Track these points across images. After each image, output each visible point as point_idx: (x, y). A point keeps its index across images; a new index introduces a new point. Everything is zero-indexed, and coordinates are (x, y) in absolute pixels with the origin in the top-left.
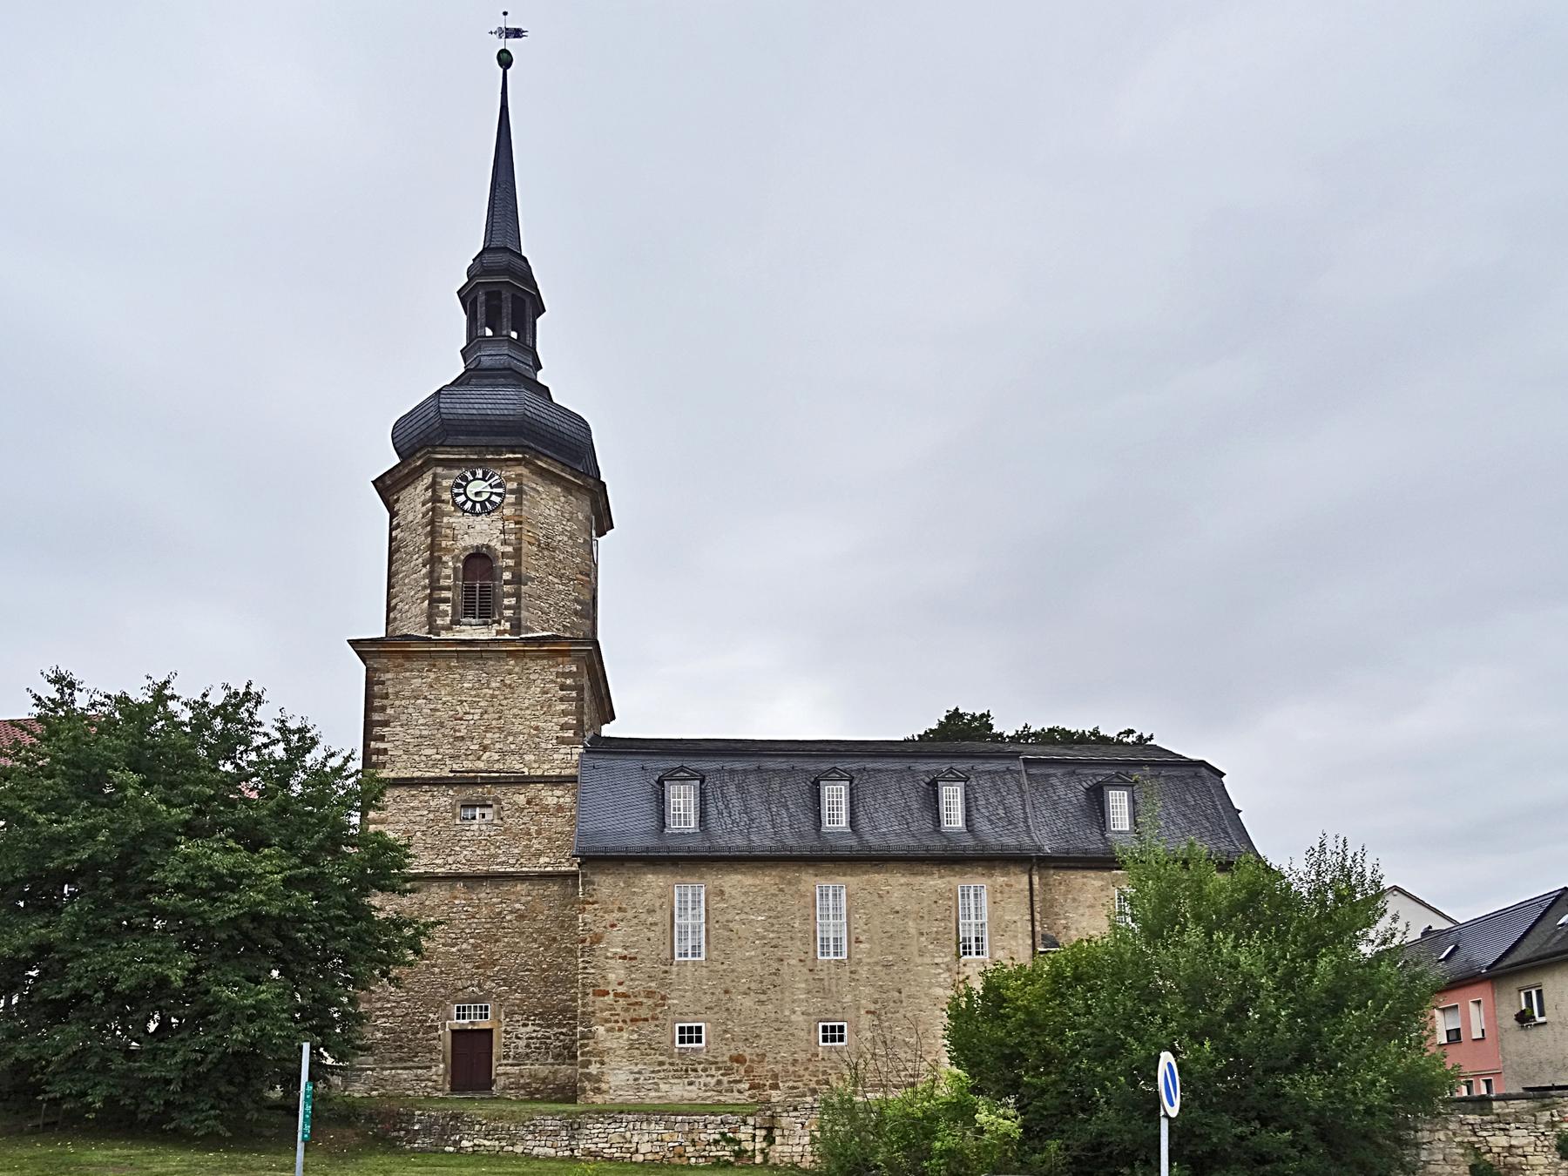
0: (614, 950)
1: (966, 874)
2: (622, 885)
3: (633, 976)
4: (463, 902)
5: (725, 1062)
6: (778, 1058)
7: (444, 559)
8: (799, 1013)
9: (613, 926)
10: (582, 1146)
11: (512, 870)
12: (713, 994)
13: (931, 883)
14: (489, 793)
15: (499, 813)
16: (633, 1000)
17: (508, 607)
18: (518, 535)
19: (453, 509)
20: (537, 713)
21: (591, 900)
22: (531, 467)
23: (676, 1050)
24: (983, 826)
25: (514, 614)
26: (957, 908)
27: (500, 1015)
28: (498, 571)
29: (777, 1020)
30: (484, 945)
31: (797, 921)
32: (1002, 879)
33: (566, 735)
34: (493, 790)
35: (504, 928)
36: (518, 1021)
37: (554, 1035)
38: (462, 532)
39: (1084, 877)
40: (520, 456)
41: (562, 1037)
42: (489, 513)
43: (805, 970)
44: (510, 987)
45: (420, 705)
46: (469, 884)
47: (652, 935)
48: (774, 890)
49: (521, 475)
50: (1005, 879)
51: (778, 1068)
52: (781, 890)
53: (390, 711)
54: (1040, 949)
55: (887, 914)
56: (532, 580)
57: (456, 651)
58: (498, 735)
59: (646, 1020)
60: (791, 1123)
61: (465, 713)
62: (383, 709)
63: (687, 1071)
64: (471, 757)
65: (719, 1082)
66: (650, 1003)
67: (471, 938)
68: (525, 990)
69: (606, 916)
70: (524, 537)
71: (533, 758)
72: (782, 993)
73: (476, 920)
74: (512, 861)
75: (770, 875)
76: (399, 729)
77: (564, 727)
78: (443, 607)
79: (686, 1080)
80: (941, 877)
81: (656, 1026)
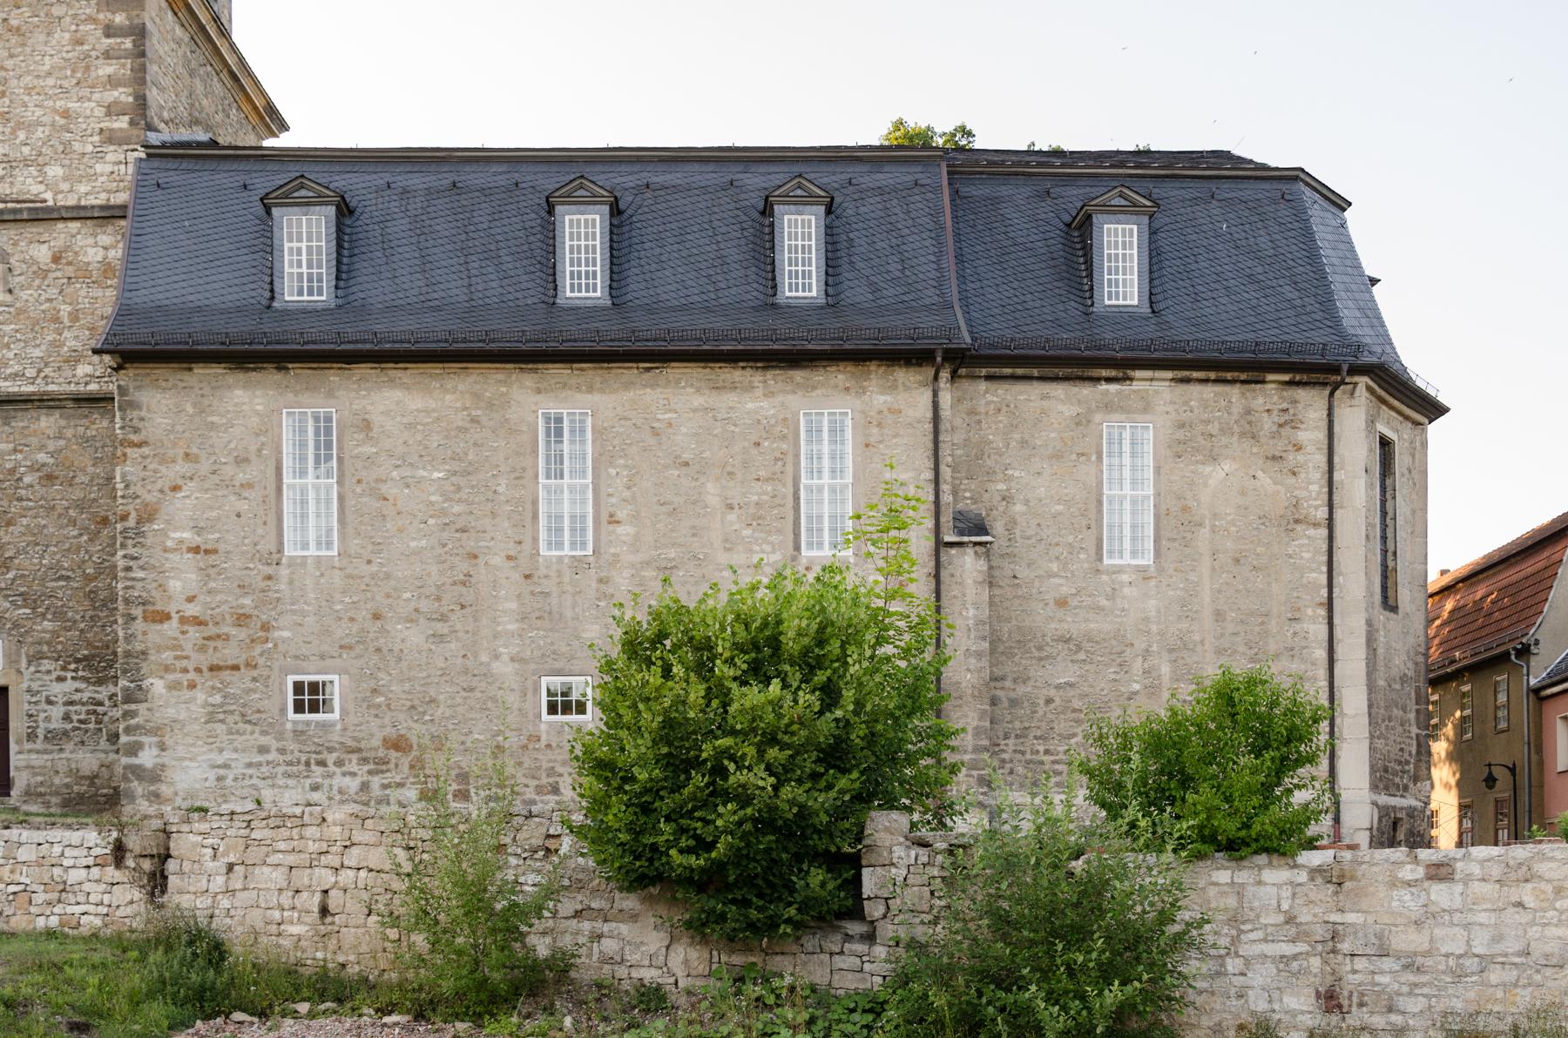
0: (177, 535)
1: (814, 388)
2: (190, 410)
3: (212, 585)
5: (376, 749)
6: (469, 744)
8: (505, 658)
9: (175, 488)
11: (31, 389)
12: (352, 619)
13: (750, 406)
16: (211, 630)
20: (65, 83)
21: (134, 438)
24: (856, 292)
26: (797, 456)
29: (466, 671)
31: (503, 482)
32: (882, 398)
33: (116, 125)
35: (20, 499)
36: (49, 672)
39: (1045, 397)
43: (517, 576)
47: (243, 506)
48: (460, 419)
50: (889, 398)
51: (466, 762)
52: (474, 420)
54: (947, 539)
55: (666, 467)
59: (236, 668)
60: (195, 845)
63: (308, 764)
65: (365, 787)
68: (59, 615)
69: (163, 469)
72: (476, 619)
74: (31, 373)
75: (455, 390)
80: (769, 394)
81: (254, 679)
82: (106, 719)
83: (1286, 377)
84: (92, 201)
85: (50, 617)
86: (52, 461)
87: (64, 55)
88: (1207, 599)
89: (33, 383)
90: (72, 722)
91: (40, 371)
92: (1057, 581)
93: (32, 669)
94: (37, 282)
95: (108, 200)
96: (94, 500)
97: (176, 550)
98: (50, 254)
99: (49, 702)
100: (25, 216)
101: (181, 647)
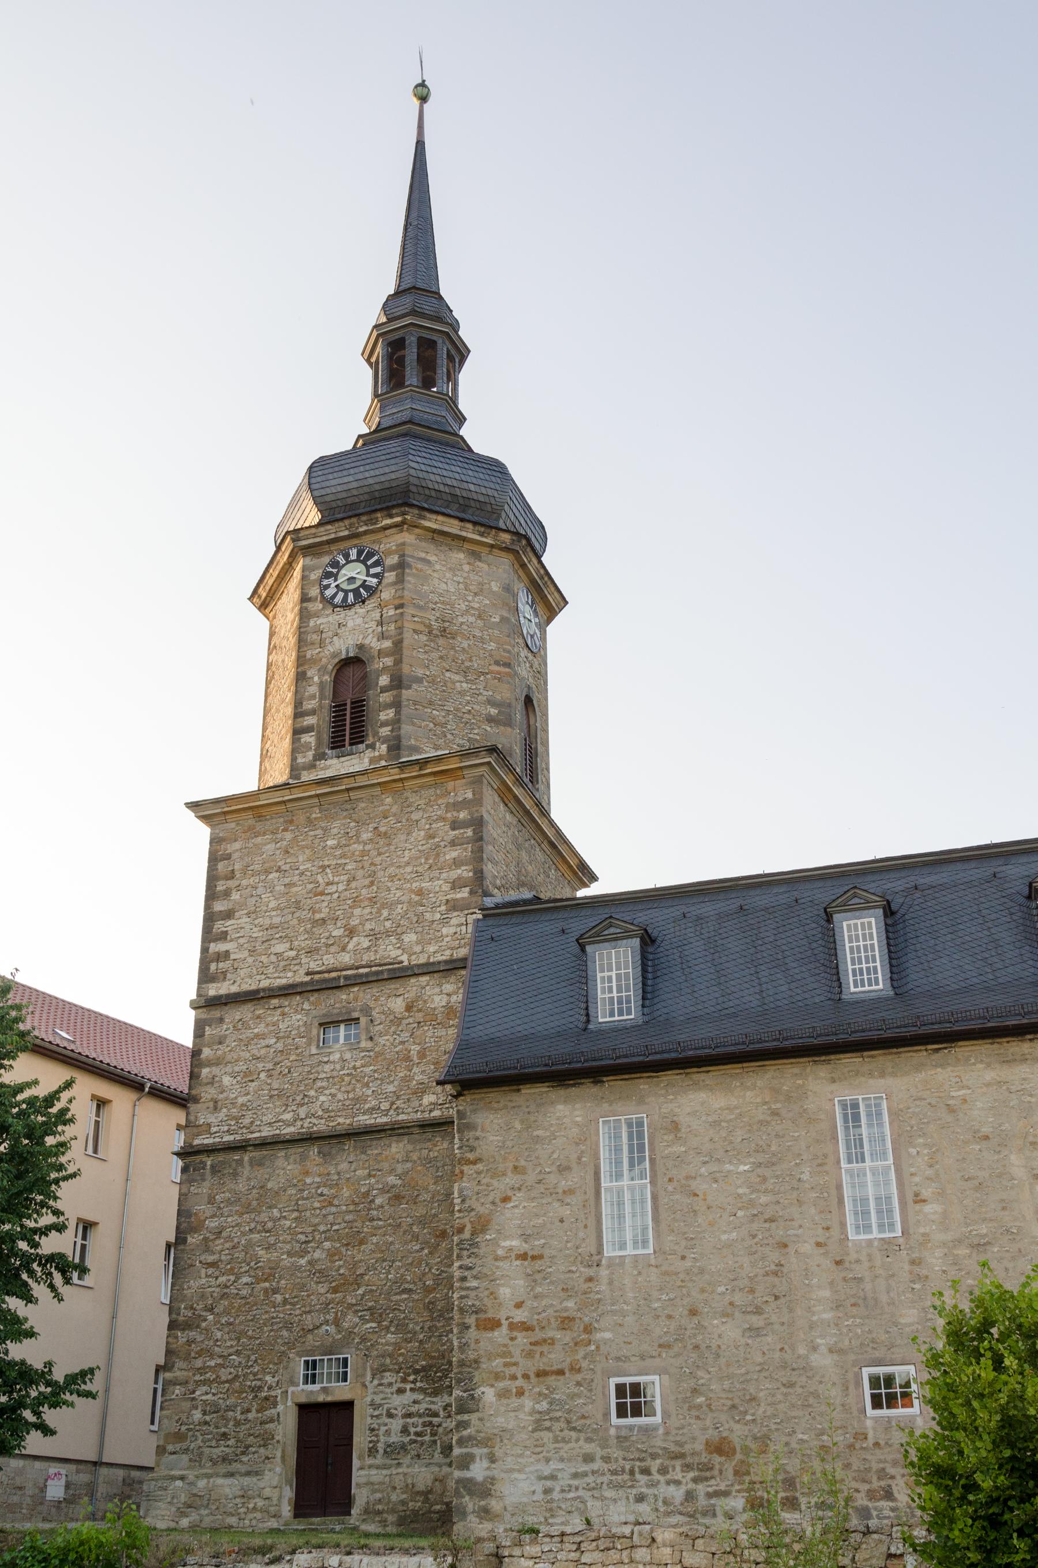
0: (507, 1243)
2: (518, 1126)
3: (538, 1289)
4: (317, 1179)
5: (699, 1454)
6: (794, 1445)
7: (309, 674)
8: (823, 1349)
9: (506, 1199)
11: (385, 1120)
12: (670, 1317)
14: (356, 999)
16: (538, 1335)
17: (384, 724)
18: (399, 624)
19: (321, 606)
20: (420, 869)
21: (471, 1156)
22: (417, 531)
25: (392, 731)
27: (364, 1375)
28: (373, 676)
29: (784, 1365)
30: (343, 1250)
33: (459, 896)
34: (361, 995)
36: (390, 1384)
38: (330, 634)
40: (399, 519)
42: (363, 602)
43: (827, 1263)
46: (326, 1149)
47: (566, 1212)
49: (403, 544)
51: (793, 1465)
52: (775, 1113)
53: (235, 896)
56: (419, 680)
57: (318, 796)
58: (368, 910)
59: (561, 1372)
61: (328, 884)
62: (227, 893)
63: (632, 1472)
64: (333, 949)
65: (690, 1496)
66: (567, 1339)
67: (326, 1239)
68: (401, 1327)
69: (495, 1183)
70: (406, 624)
72: (791, 1310)
73: (333, 1209)
74: (385, 1106)
76: (245, 919)
77: (456, 885)
81: (578, 1384)
82: (441, 1430)
86: (399, 1182)
89: (386, 1115)
90: (409, 1434)
91: (393, 1103)
93: (376, 1382)
94: (393, 1029)
96: (435, 1215)
98: (404, 1004)
99: (390, 1415)
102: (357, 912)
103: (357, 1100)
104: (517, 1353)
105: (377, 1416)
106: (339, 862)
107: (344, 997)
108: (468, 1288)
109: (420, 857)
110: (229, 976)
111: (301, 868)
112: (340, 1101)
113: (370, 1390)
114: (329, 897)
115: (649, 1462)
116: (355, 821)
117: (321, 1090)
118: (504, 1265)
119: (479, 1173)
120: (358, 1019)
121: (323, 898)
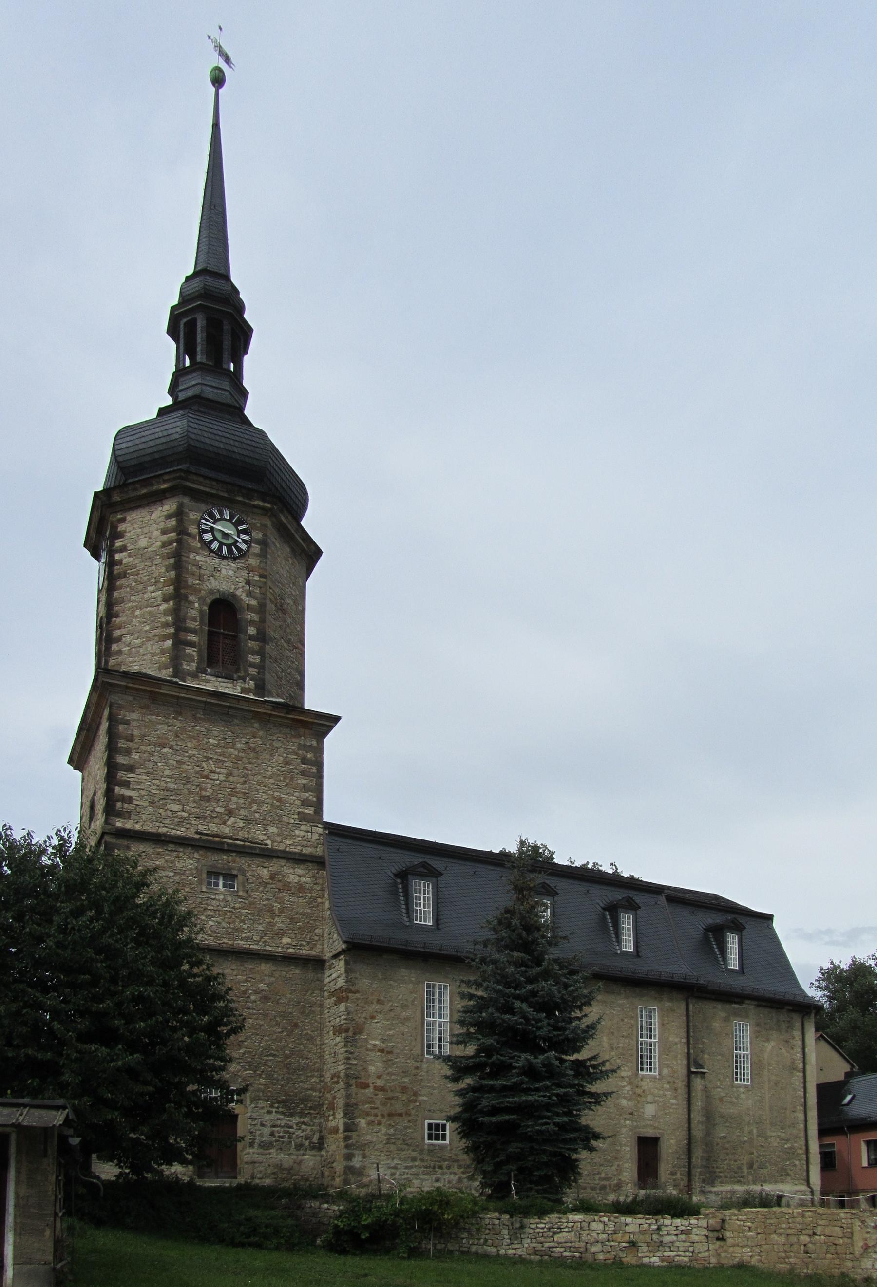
0: (373, 1042)
3: (390, 1070)
7: (191, 598)
9: (373, 1017)
10: (526, 1245)
11: (256, 947)
15: (244, 886)
16: (390, 1094)
19: (199, 545)
21: (353, 988)
23: (426, 1147)
25: (258, 673)
33: (307, 811)
36: (262, 1108)
37: (297, 1124)
40: (269, 505)
41: (303, 1127)
44: (255, 1071)
45: (166, 753)
53: (135, 756)
54: (693, 1070)
57: (205, 702)
59: (400, 1115)
61: (211, 772)
62: (128, 752)
66: (404, 1098)
68: (269, 1076)
71: (275, 830)
74: (256, 938)
76: (144, 777)
78: (190, 651)
79: (434, 1177)
82: (294, 1136)
83: (791, 1008)
84: (293, 849)
85: (264, 1076)
86: (267, 989)
87: (279, 768)
88: (767, 1101)
89: (257, 944)
90: (275, 1137)
91: (262, 938)
92: (719, 1090)
93: (253, 1106)
94: (261, 889)
95: (302, 850)
96: (290, 1013)
97: (373, 1050)
98: (268, 874)
99: (262, 1125)
100: (257, 851)
101: (373, 1102)
102: (234, 799)
103: (236, 930)
104: (378, 1104)
105: (255, 1125)
106: (220, 758)
107: (225, 857)
108: (351, 1064)
109: (279, 775)
110: (133, 816)
111: (190, 752)
112: (224, 928)
113: (250, 1110)
114: (212, 782)
115: (442, 1163)
116: (231, 731)
117: (209, 917)
118: (372, 1054)
119: (358, 999)
120: (236, 876)
121: (207, 781)
